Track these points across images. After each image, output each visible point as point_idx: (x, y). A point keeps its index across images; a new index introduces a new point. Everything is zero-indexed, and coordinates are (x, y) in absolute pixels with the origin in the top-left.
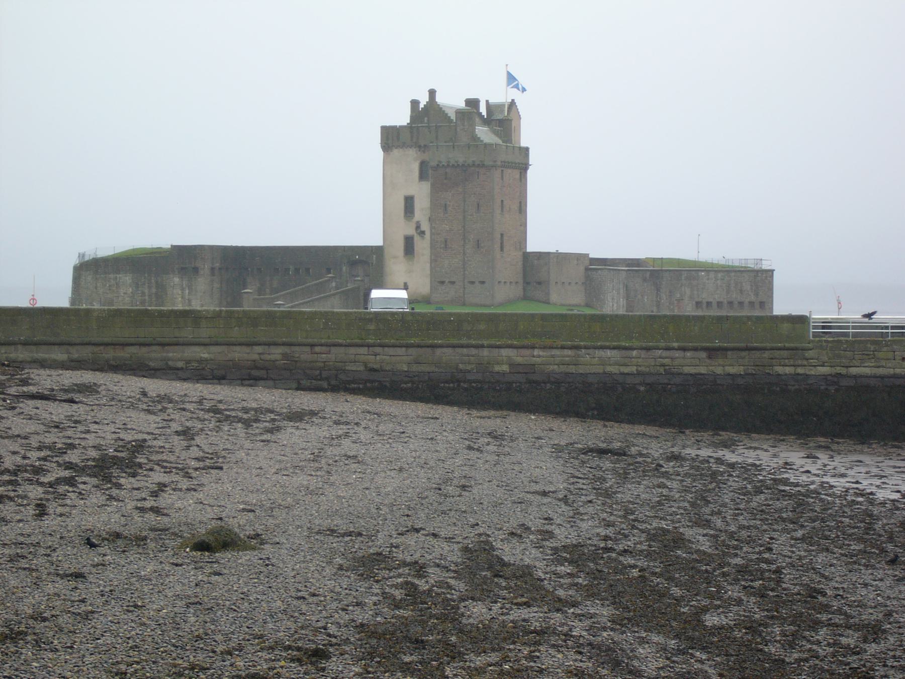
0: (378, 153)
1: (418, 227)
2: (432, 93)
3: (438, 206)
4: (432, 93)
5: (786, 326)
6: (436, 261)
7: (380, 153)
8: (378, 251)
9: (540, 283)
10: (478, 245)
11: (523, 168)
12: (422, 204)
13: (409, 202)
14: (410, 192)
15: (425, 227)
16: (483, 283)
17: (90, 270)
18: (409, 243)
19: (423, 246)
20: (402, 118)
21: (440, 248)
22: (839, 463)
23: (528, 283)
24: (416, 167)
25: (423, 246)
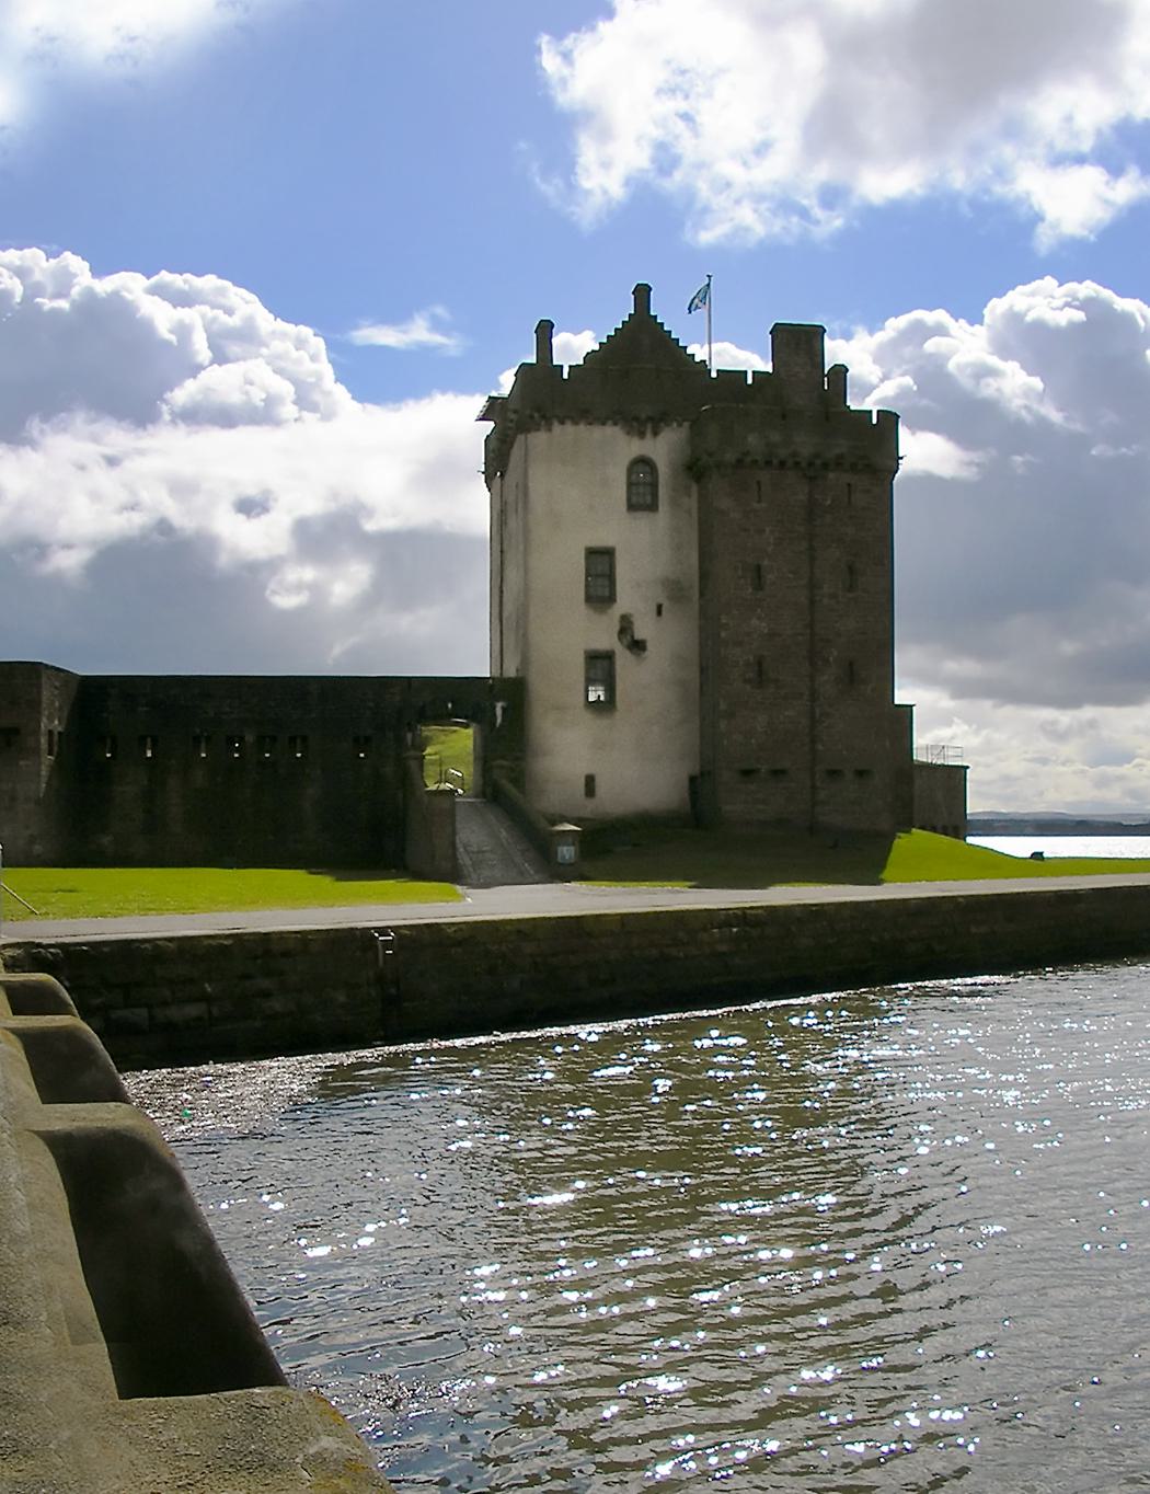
2: (642, 293)
3: (707, 591)
4: (642, 293)
15: (668, 640)
21: (713, 680)
25: (650, 682)
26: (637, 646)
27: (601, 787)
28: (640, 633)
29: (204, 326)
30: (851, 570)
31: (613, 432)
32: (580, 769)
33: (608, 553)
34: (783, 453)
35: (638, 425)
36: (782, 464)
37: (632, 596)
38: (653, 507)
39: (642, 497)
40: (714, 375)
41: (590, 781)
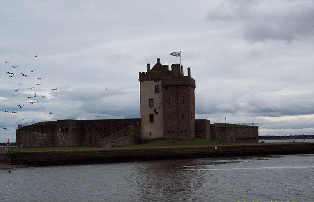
0: (138, 83)
1: (155, 111)
2: (158, 60)
3: (166, 103)
4: (158, 60)
5: (43, 136)
6: (166, 123)
7: (139, 83)
8: (139, 120)
9: (202, 131)
10: (183, 116)
11: (194, 87)
12: (156, 105)
13: (151, 100)
14: (152, 98)
15: (160, 111)
16: (186, 131)
17: (23, 131)
18: (151, 117)
19: (158, 118)
20: (145, 70)
21: (167, 118)
22: (205, 161)
23: (197, 132)
24: (153, 88)
25: (158, 118)
26: (157, 113)
27: (152, 134)
28: (157, 111)
29: (136, 144)
30: (183, 100)
31: (153, 82)
32: (149, 131)
33: (152, 99)
34: (173, 84)
35: (156, 80)
36: (172, 86)
37: (156, 105)
38: (159, 92)
39: (157, 91)
40: (170, 69)
41: (150, 133)
